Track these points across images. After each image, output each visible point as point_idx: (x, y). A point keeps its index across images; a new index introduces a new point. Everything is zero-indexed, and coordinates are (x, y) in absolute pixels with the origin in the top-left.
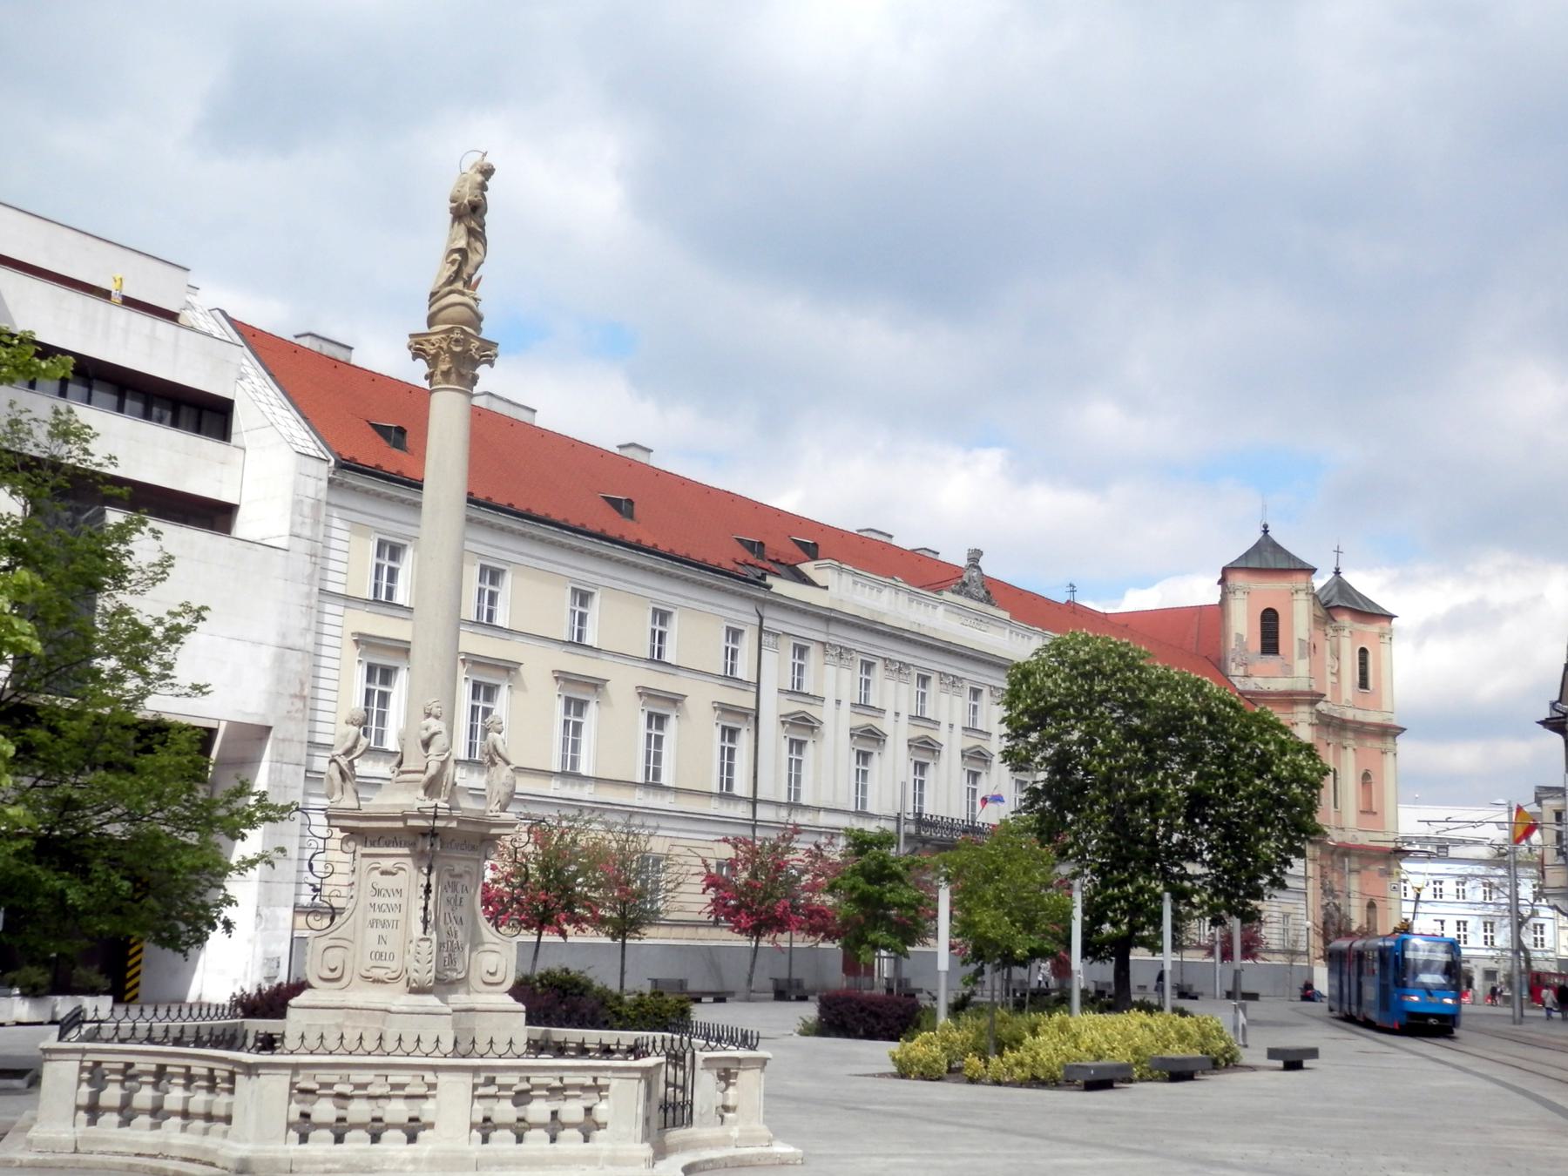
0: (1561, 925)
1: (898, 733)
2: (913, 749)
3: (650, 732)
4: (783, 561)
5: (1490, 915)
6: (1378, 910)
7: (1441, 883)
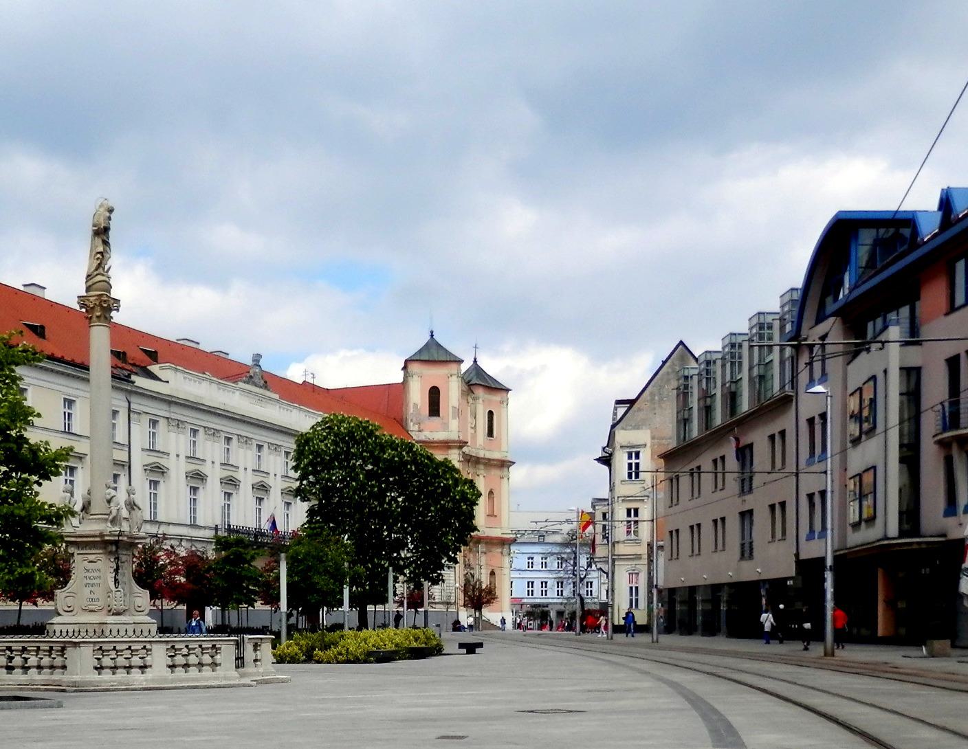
0: (602, 581)
1: (214, 474)
2: (223, 484)
3: (66, 478)
4: (137, 364)
5: (561, 578)
6: (496, 576)
7: (532, 558)
